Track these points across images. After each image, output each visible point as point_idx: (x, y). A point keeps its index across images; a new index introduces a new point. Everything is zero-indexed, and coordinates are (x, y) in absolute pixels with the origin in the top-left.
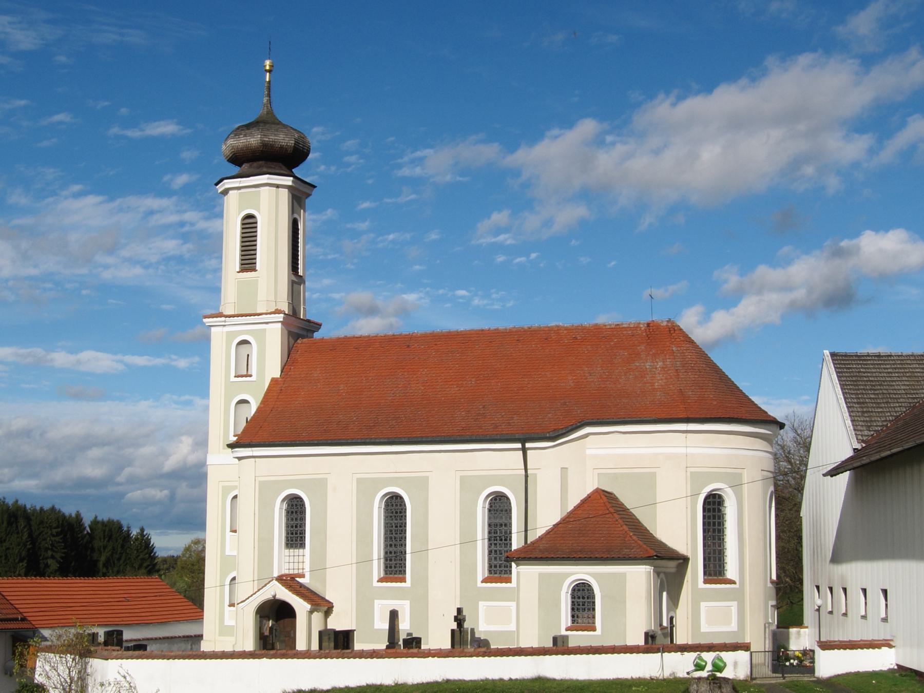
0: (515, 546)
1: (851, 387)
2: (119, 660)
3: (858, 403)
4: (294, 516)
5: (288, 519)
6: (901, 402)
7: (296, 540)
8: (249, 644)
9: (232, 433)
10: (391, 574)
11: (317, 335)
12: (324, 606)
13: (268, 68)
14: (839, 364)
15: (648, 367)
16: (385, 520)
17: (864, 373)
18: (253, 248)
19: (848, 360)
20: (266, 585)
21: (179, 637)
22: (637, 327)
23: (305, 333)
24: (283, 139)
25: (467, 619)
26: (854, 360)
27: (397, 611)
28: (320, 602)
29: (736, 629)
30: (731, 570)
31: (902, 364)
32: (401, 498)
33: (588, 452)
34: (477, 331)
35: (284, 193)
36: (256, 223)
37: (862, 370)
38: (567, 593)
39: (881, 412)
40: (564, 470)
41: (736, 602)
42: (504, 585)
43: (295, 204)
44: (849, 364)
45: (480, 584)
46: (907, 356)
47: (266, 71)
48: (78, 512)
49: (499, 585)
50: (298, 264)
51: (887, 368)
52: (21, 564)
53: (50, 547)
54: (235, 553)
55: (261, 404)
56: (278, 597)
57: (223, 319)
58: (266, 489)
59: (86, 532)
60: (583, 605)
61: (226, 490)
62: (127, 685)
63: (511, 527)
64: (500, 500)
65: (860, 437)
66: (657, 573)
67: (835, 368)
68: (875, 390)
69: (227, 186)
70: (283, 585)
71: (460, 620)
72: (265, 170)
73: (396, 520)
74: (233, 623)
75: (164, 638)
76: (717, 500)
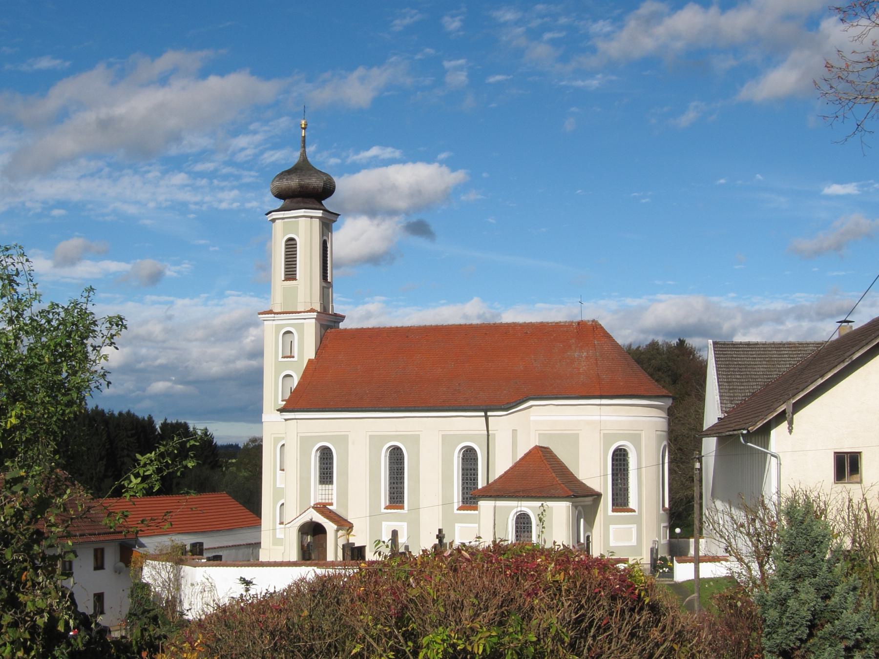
0: (480, 487)
1: (724, 369)
2: (204, 568)
3: (727, 382)
4: (325, 461)
5: (320, 464)
6: (758, 382)
7: (327, 479)
8: (294, 556)
9: (280, 399)
10: (394, 503)
11: (342, 326)
12: (347, 526)
13: (303, 126)
14: (718, 351)
15: (576, 356)
16: (390, 465)
17: (735, 358)
18: (294, 263)
19: (725, 348)
20: (305, 512)
21: (244, 545)
22: (570, 325)
23: (332, 324)
24: (315, 182)
25: (446, 536)
26: (730, 348)
27: (397, 531)
28: (343, 523)
29: (635, 544)
30: (633, 503)
31: (764, 351)
32: (401, 449)
33: (532, 418)
34: (456, 325)
35: (316, 222)
36: (296, 244)
37: (734, 356)
38: (513, 520)
39: (743, 389)
40: (514, 431)
41: (635, 525)
42: (472, 512)
43: (324, 228)
44: (726, 351)
45: (456, 511)
46: (769, 344)
47: (302, 128)
48: (150, 415)
49: (469, 512)
50: (327, 273)
51: (753, 354)
52: (101, 462)
53: (126, 447)
54: (283, 486)
55: (301, 379)
56: (314, 520)
57: (273, 315)
58: (305, 442)
59: (157, 433)
60: (524, 528)
61: (277, 440)
62: (209, 585)
63: (477, 470)
64: (470, 451)
65: (724, 409)
66: (575, 506)
67: (715, 354)
68: (742, 372)
69: (274, 217)
70: (317, 512)
71: (440, 537)
72: (302, 205)
73: (398, 465)
74: (282, 536)
75: (232, 546)
76: (622, 452)
